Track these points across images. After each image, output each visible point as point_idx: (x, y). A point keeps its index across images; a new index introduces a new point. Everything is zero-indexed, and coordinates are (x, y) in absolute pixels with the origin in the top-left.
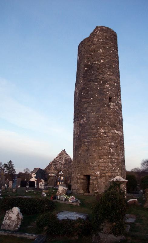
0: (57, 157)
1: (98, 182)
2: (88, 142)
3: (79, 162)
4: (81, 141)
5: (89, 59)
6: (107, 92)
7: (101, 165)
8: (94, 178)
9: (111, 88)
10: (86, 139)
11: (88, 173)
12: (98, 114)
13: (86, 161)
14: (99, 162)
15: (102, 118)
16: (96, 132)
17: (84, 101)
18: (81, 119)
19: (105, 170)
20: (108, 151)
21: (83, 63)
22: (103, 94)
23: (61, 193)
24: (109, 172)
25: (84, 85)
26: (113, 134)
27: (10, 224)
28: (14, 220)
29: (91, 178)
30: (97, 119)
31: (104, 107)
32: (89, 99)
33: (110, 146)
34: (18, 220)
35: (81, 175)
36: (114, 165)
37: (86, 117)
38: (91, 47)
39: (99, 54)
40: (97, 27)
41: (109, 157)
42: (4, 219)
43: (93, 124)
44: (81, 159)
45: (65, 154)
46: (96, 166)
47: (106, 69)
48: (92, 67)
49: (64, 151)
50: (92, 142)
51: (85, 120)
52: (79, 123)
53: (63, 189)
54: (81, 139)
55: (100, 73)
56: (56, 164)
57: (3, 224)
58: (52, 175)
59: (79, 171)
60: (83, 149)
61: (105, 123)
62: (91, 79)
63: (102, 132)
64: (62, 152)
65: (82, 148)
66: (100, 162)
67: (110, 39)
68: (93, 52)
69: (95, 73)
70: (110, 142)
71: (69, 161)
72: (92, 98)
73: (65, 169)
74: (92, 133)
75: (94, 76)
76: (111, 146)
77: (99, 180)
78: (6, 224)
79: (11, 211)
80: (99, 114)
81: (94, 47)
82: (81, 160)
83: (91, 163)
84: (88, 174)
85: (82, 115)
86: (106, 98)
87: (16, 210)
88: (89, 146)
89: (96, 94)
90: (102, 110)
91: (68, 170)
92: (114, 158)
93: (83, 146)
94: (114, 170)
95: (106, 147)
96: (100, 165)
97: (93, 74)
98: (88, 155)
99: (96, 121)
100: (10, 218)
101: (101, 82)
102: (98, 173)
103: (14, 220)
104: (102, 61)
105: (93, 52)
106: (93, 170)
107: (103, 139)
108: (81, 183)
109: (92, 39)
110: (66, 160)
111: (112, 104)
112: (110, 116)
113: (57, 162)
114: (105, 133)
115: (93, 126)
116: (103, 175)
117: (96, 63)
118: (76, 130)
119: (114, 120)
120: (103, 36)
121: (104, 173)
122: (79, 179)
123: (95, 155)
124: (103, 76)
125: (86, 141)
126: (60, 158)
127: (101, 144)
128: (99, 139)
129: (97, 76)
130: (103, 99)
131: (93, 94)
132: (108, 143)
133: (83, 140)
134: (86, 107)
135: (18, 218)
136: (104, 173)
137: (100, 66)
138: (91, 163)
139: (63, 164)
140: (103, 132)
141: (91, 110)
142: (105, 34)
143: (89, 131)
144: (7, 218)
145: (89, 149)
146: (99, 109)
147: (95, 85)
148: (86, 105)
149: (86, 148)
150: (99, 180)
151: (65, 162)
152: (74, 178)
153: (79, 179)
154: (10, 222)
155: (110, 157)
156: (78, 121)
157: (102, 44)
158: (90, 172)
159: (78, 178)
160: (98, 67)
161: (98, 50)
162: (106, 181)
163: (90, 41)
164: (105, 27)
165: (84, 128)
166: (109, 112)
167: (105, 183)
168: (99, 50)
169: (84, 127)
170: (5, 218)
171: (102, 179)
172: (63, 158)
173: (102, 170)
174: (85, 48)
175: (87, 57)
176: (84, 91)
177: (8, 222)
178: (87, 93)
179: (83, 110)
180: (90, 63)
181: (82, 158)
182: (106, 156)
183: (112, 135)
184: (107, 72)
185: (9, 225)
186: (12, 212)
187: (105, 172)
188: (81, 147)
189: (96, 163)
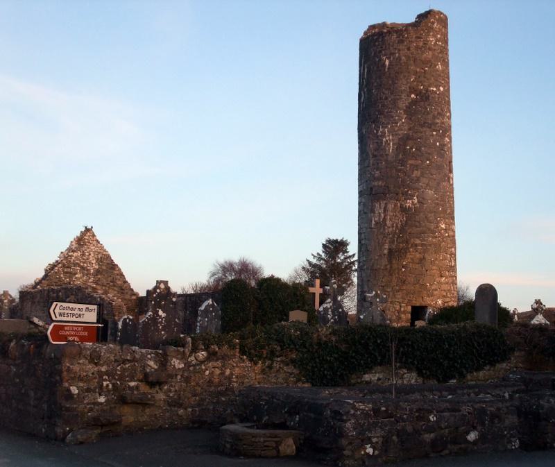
0: (70, 250)
11: (423, 303)
14: (439, 283)
17: (411, 165)
18: (406, 199)
19: (447, 297)
25: (410, 129)
30: (435, 203)
32: (423, 162)
46: (436, 290)
48: (427, 98)
50: (430, 245)
52: (399, 205)
55: (439, 113)
56: (70, 273)
59: (402, 298)
60: (411, 256)
61: (446, 211)
62: (425, 123)
63: (442, 229)
65: (408, 256)
72: (428, 162)
74: (429, 229)
75: (430, 116)
81: (429, 55)
85: (410, 192)
97: (428, 113)
104: (442, 89)
110: (99, 261)
113: (76, 264)
123: (435, 269)
126: (83, 255)
129: (434, 117)
131: (429, 154)
137: (438, 98)
139: (92, 271)
141: (428, 185)
145: (424, 258)
146: (438, 184)
147: (433, 135)
148: (416, 173)
149: (418, 255)
151: (97, 267)
156: (397, 200)
169: (414, 214)
172: (92, 255)
174: (409, 49)
178: (418, 149)
189: (436, 285)
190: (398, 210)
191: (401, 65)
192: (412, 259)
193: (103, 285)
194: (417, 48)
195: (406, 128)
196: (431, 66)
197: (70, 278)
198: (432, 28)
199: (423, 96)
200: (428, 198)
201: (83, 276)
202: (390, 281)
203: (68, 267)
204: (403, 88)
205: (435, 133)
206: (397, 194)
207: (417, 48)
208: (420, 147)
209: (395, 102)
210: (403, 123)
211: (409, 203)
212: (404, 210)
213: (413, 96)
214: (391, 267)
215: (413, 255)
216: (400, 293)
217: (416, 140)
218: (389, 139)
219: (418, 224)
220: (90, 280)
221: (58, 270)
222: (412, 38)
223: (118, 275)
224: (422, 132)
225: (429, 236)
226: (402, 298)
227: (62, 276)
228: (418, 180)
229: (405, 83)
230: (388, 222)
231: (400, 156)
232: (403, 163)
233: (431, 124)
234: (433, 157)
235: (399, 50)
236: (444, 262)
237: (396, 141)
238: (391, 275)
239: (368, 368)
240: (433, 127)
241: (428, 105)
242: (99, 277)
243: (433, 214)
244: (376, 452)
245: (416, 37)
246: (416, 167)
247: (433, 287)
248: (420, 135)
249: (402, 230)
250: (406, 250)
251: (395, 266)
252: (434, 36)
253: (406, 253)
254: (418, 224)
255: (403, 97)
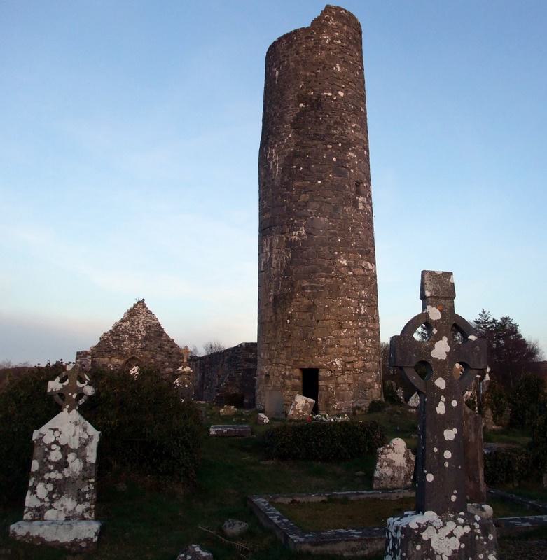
0: (122, 321)
1: (338, 384)
2: (312, 288)
3: (289, 337)
4: (292, 286)
5: (309, 82)
6: (352, 171)
7: (343, 342)
8: (329, 373)
9: (358, 160)
10: (305, 279)
11: (313, 364)
12: (334, 220)
13: (307, 334)
14: (337, 337)
15: (342, 232)
16: (330, 264)
17: (298, 187)
18: (291, 231)
19: (351, 355)
20: (356, 311)
21: (292, 90)
22: (344, 174)
23: (301, 411)
24: (359, 360)
25: (297, 145)
26: (364, 271)
27: (394, 476)
28: (401, 467)
29: (321, 374)
30: (331, 233)
31: (347, 205)
32: (313, 183)
33: (359, 299)
34: (409, 465)
35: (293, 368)
36: (368, 344)
37: (305, 228)
38: (315, 53)
39: (336, 76)
40: (328, 9)
41: (358, 325)
42: (377, 467)
43: (323, 245)
44: (295, 330)
45: (144, 313)
46: (332, 346)
47: (349, 115)
48: (320, 105)
49: (142, 303)
50: (323, 288)
51: (303, 232)
53: (307, 401)
54: (294, 280)
55: (336, 123)
56: (119, 340)
57: (377, 478)
58: (185, 370)
59: (287, 358)
60: (298, 303)
61: (349, 244)
62: (316, 135)
63: (343, 266)
64: (135, 305)
65: (295, 303)
66: (341, 337)
67: (355, 42)
68: (321, 67)
69: (325, 121)
70: (360, 290)
71: (156, 331)
72: (319, 182)
73: (146, 353)
74: (321, 266)
75: (323, 127)
76: (362, 299)
77: (340, 380)
78: (384, 476)
79: (389, 448)
80: (336, 222)
81: (322, 55)
82: (294, 333)
83: (320, 339)
84: (314, 365)
85: (296, 221)
86: (349, 185)
87: (399, 444)
88: (314, 297)
89: (328, 172)
90: (343, 213)
91: (153, 357)
92: (367, 327)
93: (300, 297)
94: (367, 355)
95: (353, 301)
96: (341, 344)
97: (320, 123)
98: (312, 318)
99: (329, 239)
100: (391, 464)
101: (340, 144)
102: (338, 362)
103: (401, 467)
104: (341, 94)
105: (321, 67)
106: (326, 354)
107: (345, 282)
108: (294, 388)
109: (317, 33)
110: (147, 329)
111: (361, 199)
112: (358, 228)
114: (349, 267)
115: (324, 250)
116: (348, 366)
117: (327, 96)
118: (274, 256)
119: (364, 237)
120: (342, 32)
121: (349, 363)
122: (289, 377)
123: (330, 320)
124: (344, 130)
125: (308, 284)
127: (342, 294)
128: (337, 281)
129: (329, 127)
130: (344, 187)
131: (321, 172)
132: (356, 291)
133: (298, 282)
134: (304, 202)
135: (408, 461)
136: (349, 363)
137: (336, 105)
138: (320, 339)
139: (140, 338)
140: (346, 264)
141: (319, 210)
142: (345, 28)
143: (313, 261)
144: (385, 464)
146: (335, 209)
147: (327, 149)
149: (306, 301)
150: (340, 380)
151: (145, 334)
152: (271, 376)
153: (289, 377)
154: (394, 472)
155: (360, 323)
156: (282, 234)
157: (341, 52)
158: (319, 361)
159: (284, 377)
160: (333, 106)
161: (332, 64)
162: (355, 380)
163: (312, 37)
164: (346, 11)
165: (302, 252)
166: (356, 219)
167: (352, 386)
168: (335, 66)
170: (378, 464)
171: (345, 376)
172: (141, 323)
173: (345, 355)
174: (297, 53)
175: (306, 76)
176: (297, 160)
177: (389, 471)
178: (307, 168)
179: (298, 209)
180: (312, 93)
181: (296, 328)
182: (353, 321)
183: (363, 273)
184: (350, 122)
185: (392, 479)
186: (393, 449)
187: (352, 359)
188: (294, 300)
189: (332, 339)
190: (283, 246)
191: (289, 72)
192: (298, 307)
193: (151, 351)
194: (307, 49)
195: (293, 144)
196: (324, 67)
197: (119, 344)
198: (326, 25)
199: (313, 104)
200: (320, 227)
201: (132, 342)
202: (275, 337)
203: (116, 335)
204: (291, 98)
205: (330, 146)
206: (282, 225)
207: (307, 49)
208: (310, 165)
209: (282, 116)
210: (290, 138)
211: (295, 236)
212: (289, 244)
213: (301, 105)
214: (276, 318)
215: (300, 301)
216: (284, 352)
217: (305, 156)
218: (276, 161)
219: (306, 261)
220: (138, 347)
221: (107, 338)
222: (301, 40)
223: (165, 341)
224: (311, 147)
225: (321, 276)
226: (287, 358)
227: (111, 343)
228: (306, 204)
229: (292, 90)
230: (274, 262)
231: (286, 179)
232: (288, 186)
233: (324, 136)
234: (327, 175)
235: (288, 56)
236: (345, 308)
237: (282, 161)
238: (276, 330)
239: (28, 484)
240: (327, 139)
241: (321, 114)
242: (147, 343)
243: (326, 248)
244: (455, 492)
245: (306, 38)
246: (304, 190)
247: (328, 342)
248: (309, 150)
249: (288, 271)
250: (291, 296)
251: (280, 317)
252: (328, 34)
253: (292, 299)
254: (306, 261)
255: (290, 108)
